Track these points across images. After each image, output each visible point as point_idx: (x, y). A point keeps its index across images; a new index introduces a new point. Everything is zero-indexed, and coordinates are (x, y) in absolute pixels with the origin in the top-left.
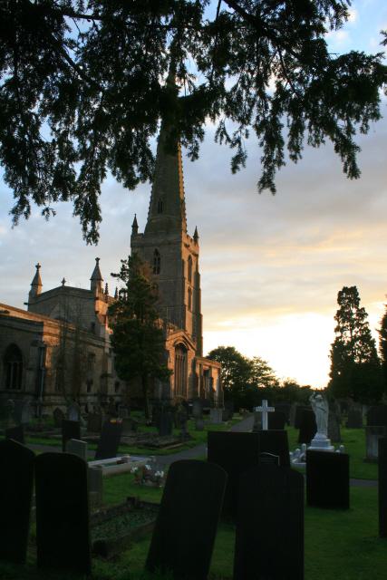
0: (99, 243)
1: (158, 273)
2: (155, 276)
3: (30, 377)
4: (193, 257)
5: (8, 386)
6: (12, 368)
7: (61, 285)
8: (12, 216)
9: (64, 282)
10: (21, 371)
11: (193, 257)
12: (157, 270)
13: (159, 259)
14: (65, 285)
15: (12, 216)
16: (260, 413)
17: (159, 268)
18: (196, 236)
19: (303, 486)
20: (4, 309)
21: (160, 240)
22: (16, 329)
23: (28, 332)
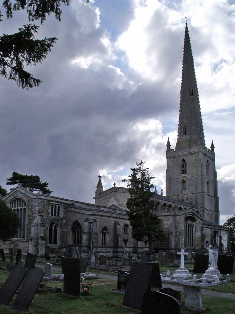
0: (163, 138)
1: (186, 173)
2: (183, 175)
3: (85, 237)
4: (210, 161)
5: (75, 242)
6: (77, 233)
7: (114, 186)
8: (51, 193)
9: (115, 184)
10: (81, 235)
11: (210, 161)
12: (184, 172)
13: (186, 164)
14: (116, 186)
15: (51, 193)
16: (180, 255)
17: (186, 170)
18: (212, 147)
19: (54, 237)
20: (71, 203)
21: (185, 153)
22: (77, 212)
23: (84, 214)
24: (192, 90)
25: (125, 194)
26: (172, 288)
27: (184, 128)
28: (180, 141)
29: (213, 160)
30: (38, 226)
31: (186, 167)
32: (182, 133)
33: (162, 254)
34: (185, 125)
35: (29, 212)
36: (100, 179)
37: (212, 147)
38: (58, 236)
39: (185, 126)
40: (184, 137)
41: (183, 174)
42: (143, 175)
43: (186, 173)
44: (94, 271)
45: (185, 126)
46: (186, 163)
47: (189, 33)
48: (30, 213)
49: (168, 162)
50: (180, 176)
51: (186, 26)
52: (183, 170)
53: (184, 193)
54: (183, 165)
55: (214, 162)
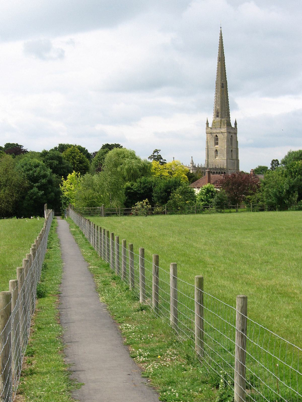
1: (218, 145)
2: (217, 146)
4: (234, 135)
12: (217, 144)
18: (236, 124)
24: (222, 88)
26: (110, 217)
29: (236, 134)
32: (216, 116)
33: (107, 151)
37: (236, 124)
40: (217, 119)
41: (216, 145)
42: (206, 188)
44: (13, 321)
50: (214, 146)
53: (217, 158)
55: (237, 135)
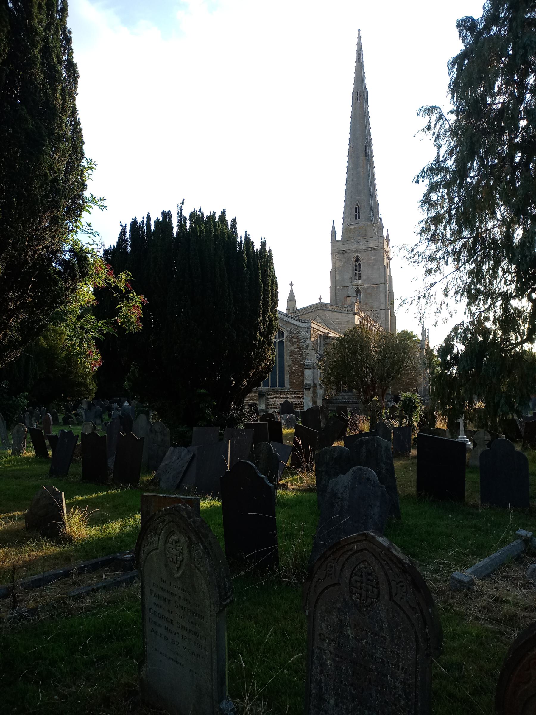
12: (358, 276)
13: (360, 265)
17: (360, 274)
25: (340, 315)
27: (356, 208)
28: (351, 227)
30: (314, 368)
31: (360, 269)
34: (359, 204)
35: (293, 347)
36: (292, 288)
37: (95, 236)
38: (287, 377)
39: (357, 205)
43: (360, 278)
45: (357, 205)
46: (361, 263)
47: (363, 47)
48: (295, 348)
49: (334, 260)
51: (359, 34)
52: (356, 274)
54: (356, 265)
